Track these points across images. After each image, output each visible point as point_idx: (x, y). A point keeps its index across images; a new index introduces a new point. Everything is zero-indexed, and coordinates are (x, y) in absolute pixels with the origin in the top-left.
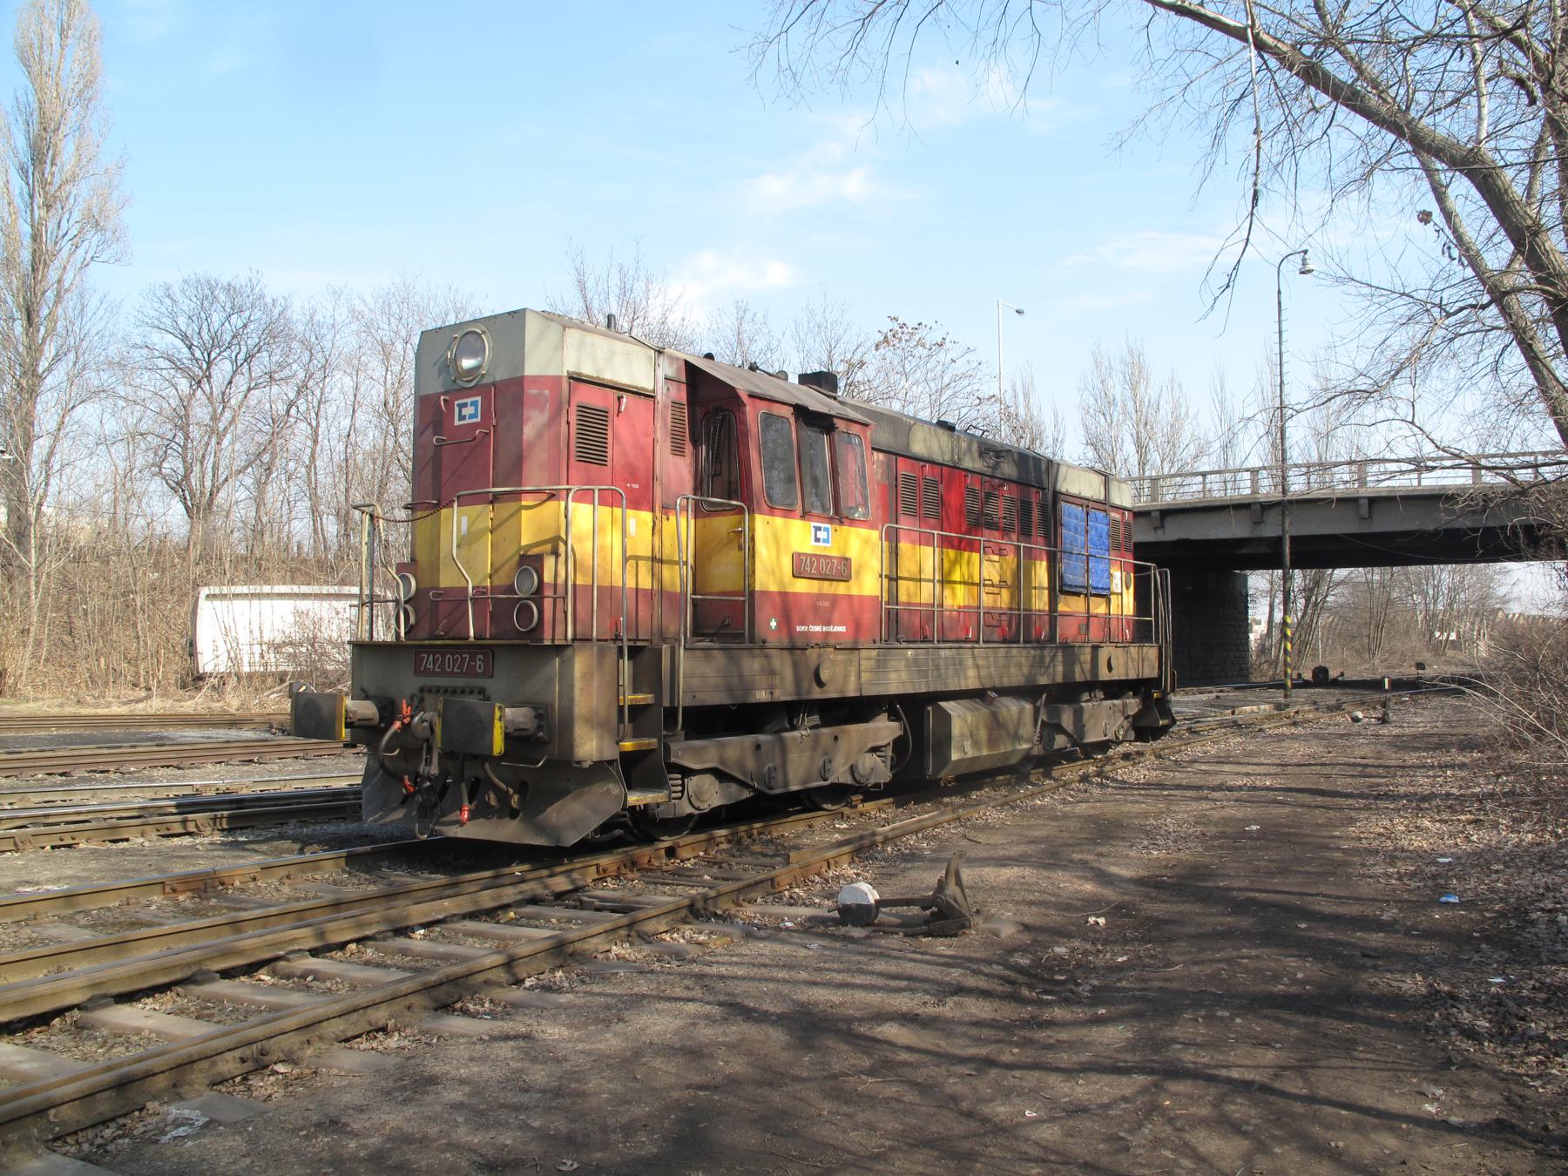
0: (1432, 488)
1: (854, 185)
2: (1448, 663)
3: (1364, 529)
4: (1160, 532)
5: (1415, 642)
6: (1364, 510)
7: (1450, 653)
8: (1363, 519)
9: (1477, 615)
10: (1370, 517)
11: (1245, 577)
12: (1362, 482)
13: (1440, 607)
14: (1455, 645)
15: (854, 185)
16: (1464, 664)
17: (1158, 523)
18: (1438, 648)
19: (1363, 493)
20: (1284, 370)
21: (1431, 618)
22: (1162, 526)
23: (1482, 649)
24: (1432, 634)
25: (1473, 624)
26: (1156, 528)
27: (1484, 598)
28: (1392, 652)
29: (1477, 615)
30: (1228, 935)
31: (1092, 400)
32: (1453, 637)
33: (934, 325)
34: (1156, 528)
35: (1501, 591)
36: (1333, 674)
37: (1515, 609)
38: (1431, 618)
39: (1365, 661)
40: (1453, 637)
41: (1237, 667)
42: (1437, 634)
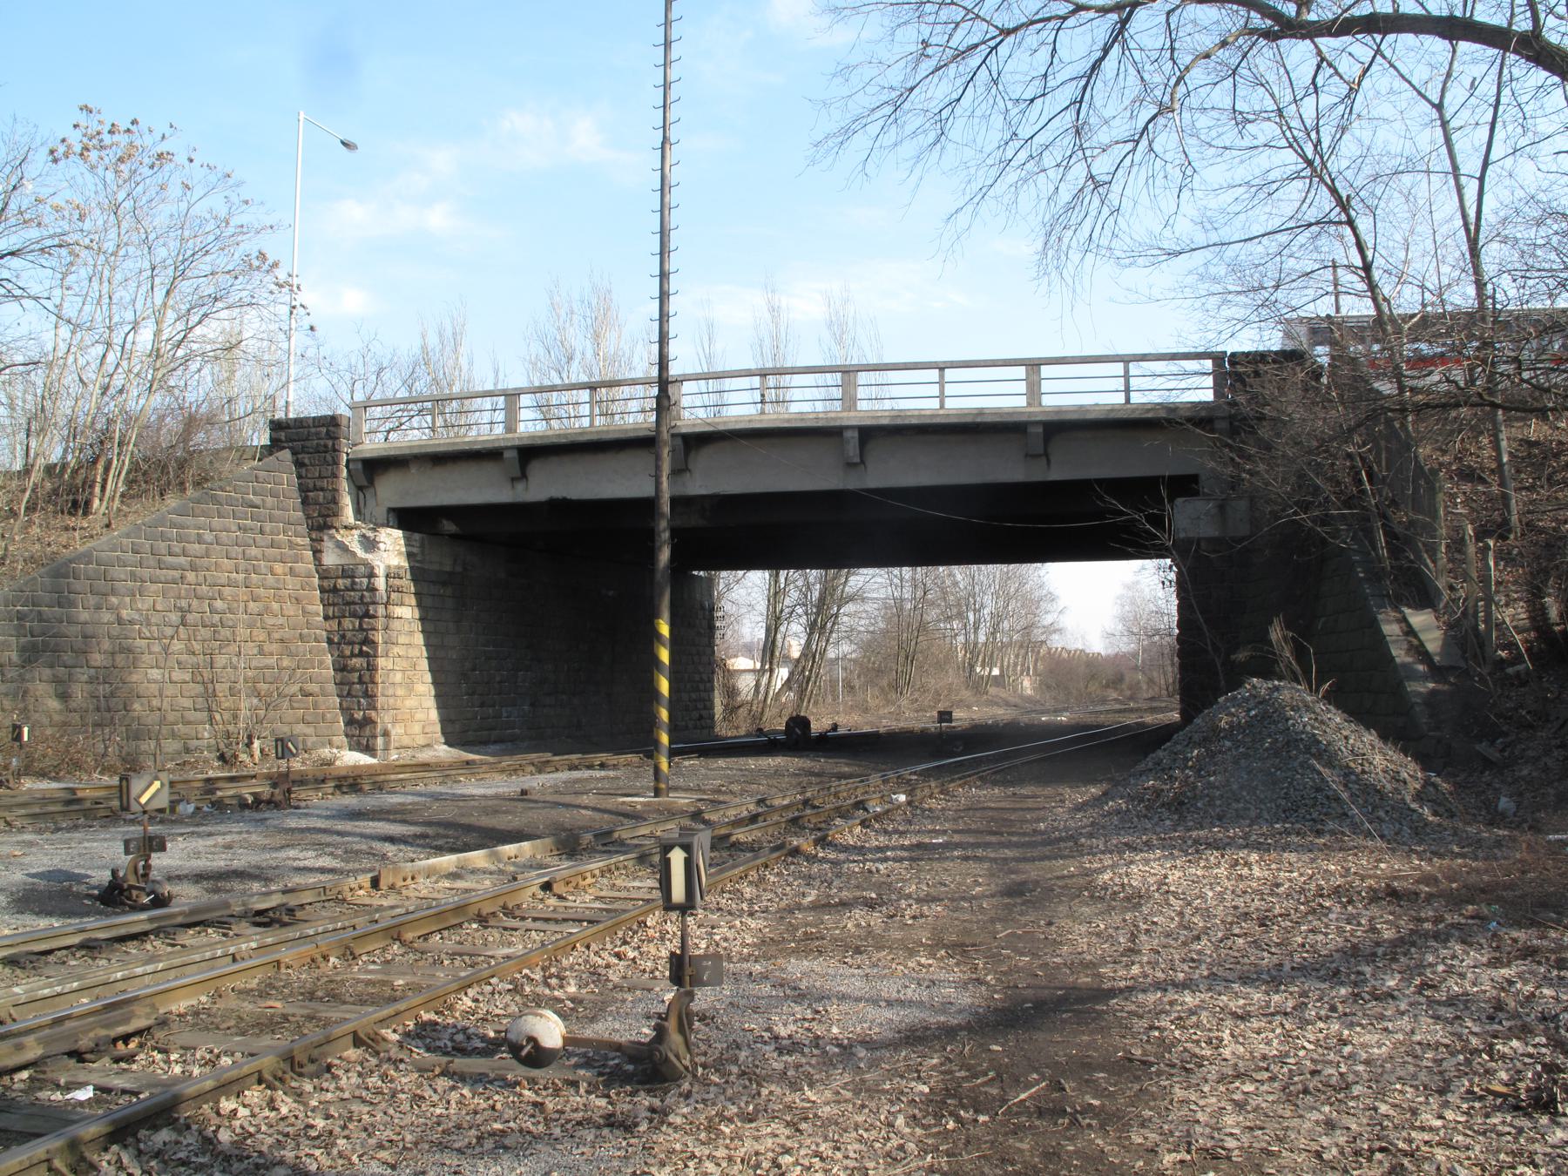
0: (963, 413)
1: (438, 219)
2: (992, 703)
3: (852, 482)
4: (520, 486)
5: (952, 677)
6: (852, 450)
7: (992, 690)
8: (850, 465)
9: (1021, 646)
10: (862, 462)
11: (710, 583)
12: (849, 400)
13: (982, 638)
14: (998, 681)
15: (438, 219)
16: (1007, 704)
17: (517, 472)
18: (978, 686)
19: (850, 419)
20: (672, 117)
21: (972, 649)
22: (524, 476)
23: (1027, 685)
24: (972, 667)
25: (1017, 656)
26: (513, 480)
27: (1028, 629)
28: (924, 689)
29: (1021, 646)
30: (1464, 216)
31: (542, 351)
32: (996, 672)
33: (168, 132)
34: (513, 480)
35: (1048, 619)
36: (818, 725)
37: (1056, 642)
38: (972, 649)
39: (888, 702)
40: (996, 672)
41: (695, 714)
42: (978, 669)
